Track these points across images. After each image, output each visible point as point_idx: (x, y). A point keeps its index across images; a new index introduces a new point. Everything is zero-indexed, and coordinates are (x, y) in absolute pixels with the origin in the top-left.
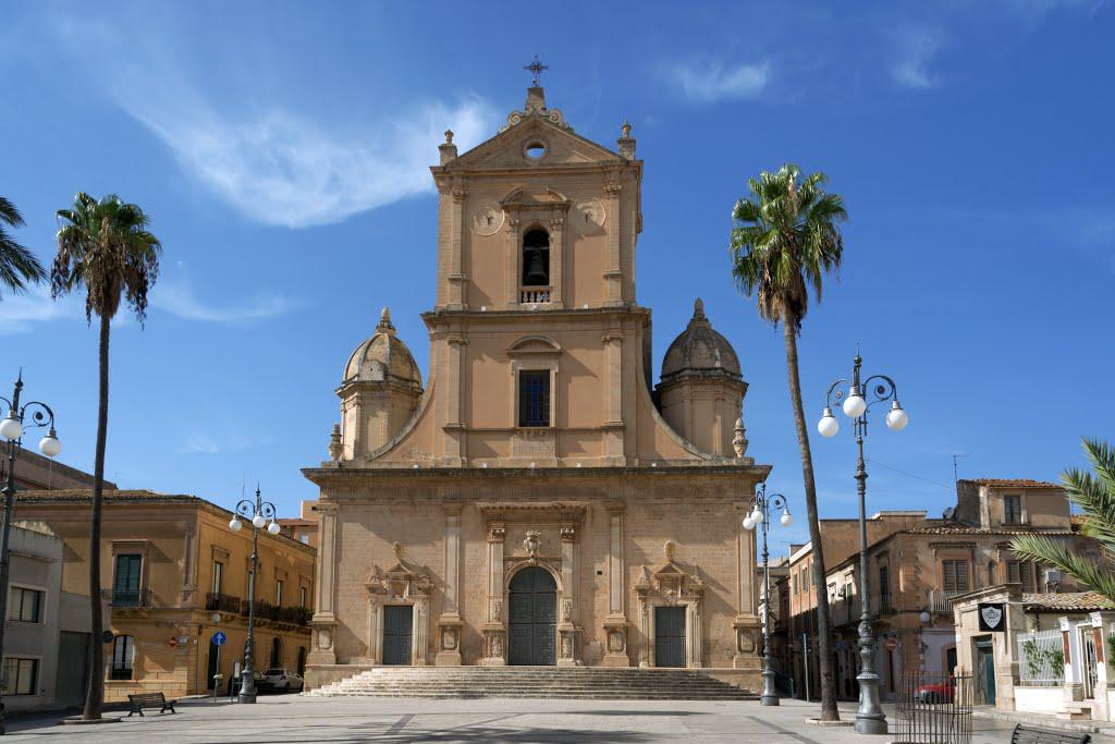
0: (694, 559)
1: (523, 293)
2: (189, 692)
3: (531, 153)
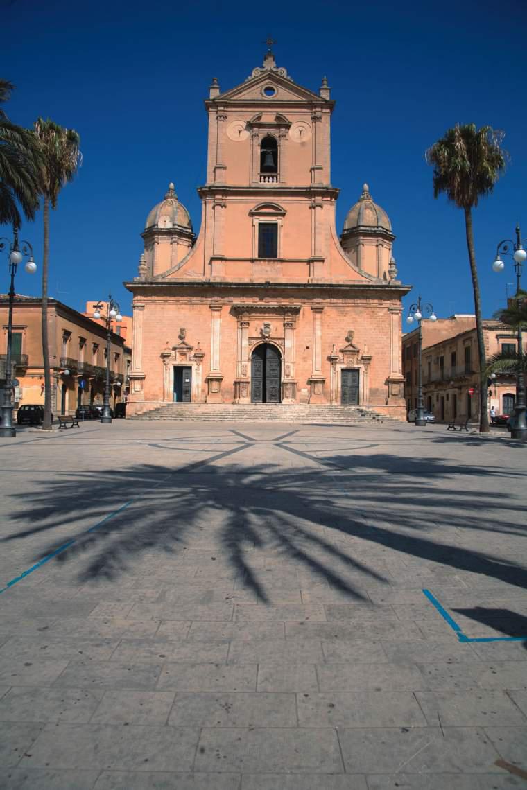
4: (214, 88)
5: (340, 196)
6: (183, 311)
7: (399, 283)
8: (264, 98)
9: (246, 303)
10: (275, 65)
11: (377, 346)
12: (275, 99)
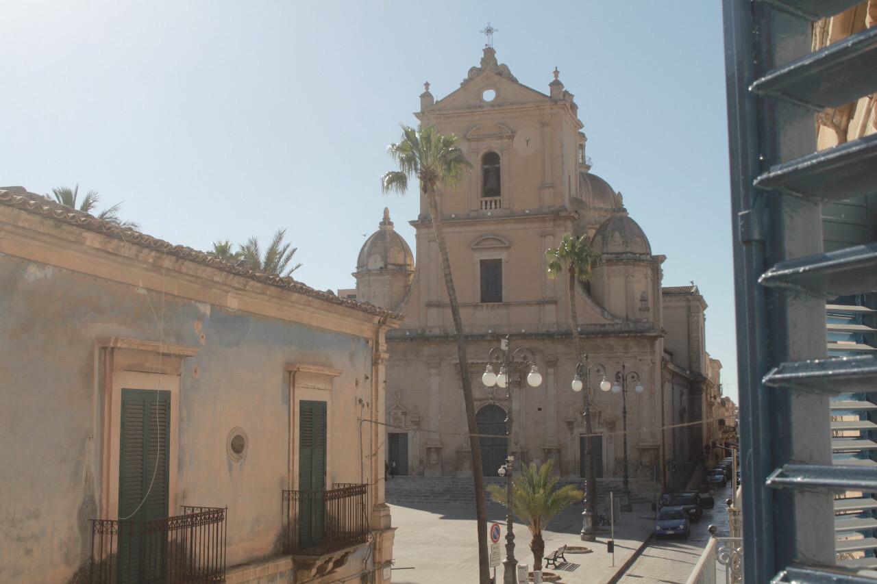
1: (481, 202)
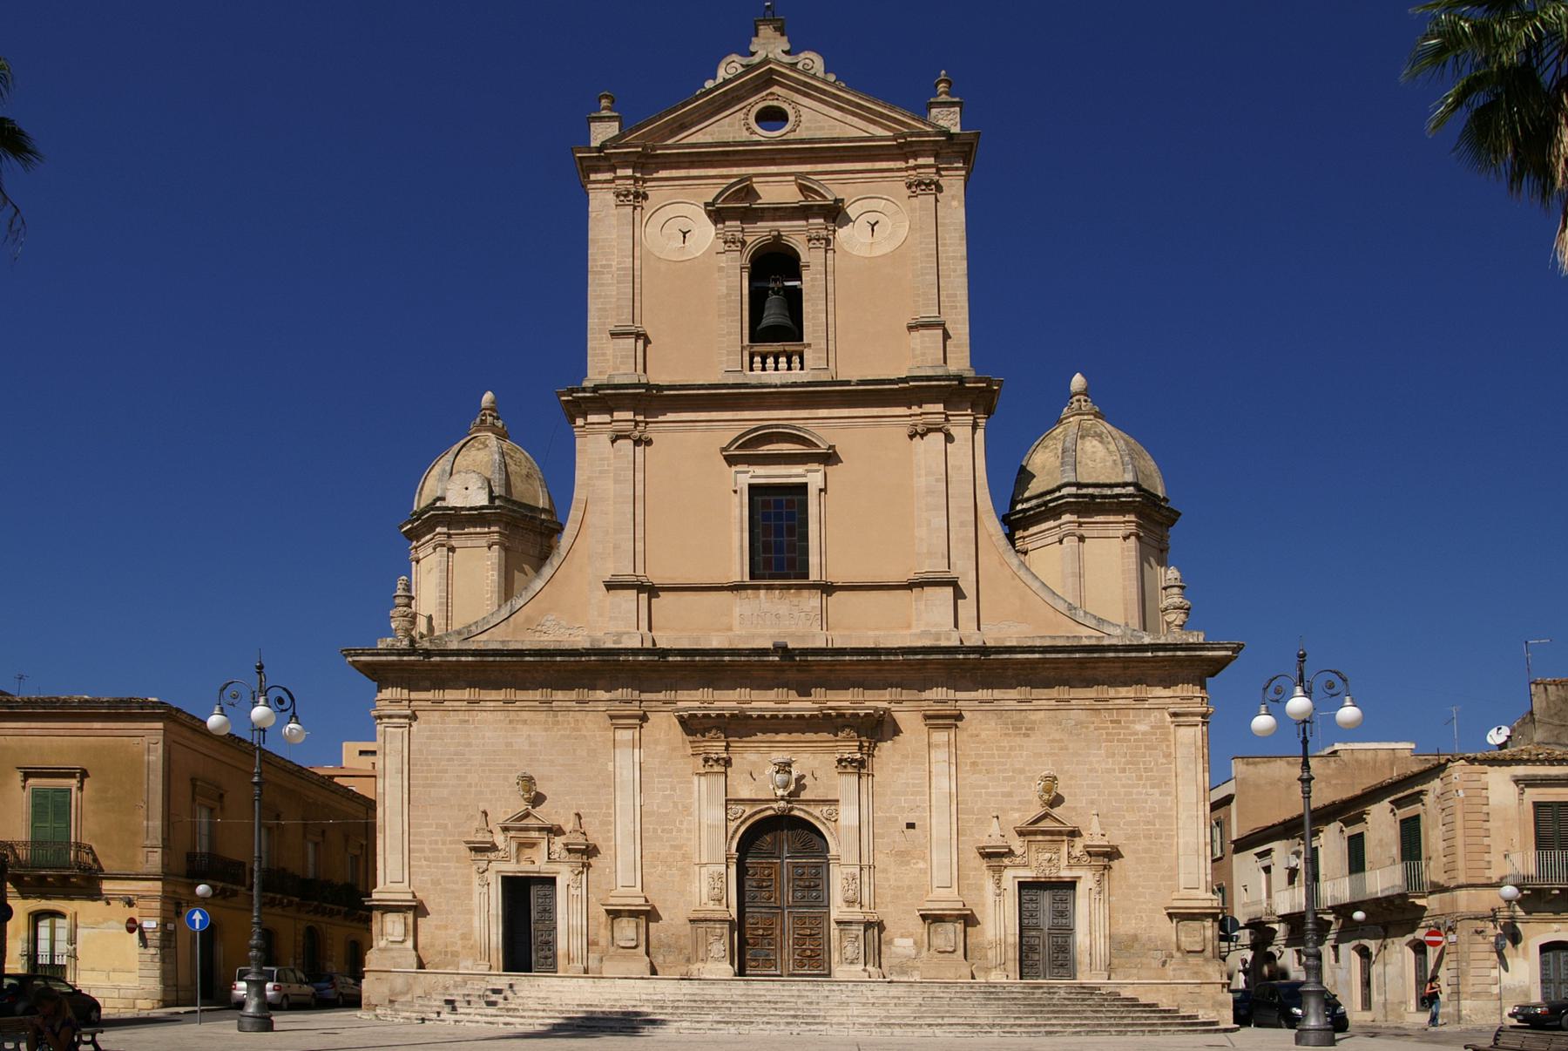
0: (1093, 802)
2: (166, 1004)
3: (769, 4)
4: (601, 119)
5: (1000, 405)
6: (525, 730)
7: (1192, 638)
8: (756, 138)
9: (717, 704)
10: (787, 47)
11: (1129, 817)
12: (791, 136)
